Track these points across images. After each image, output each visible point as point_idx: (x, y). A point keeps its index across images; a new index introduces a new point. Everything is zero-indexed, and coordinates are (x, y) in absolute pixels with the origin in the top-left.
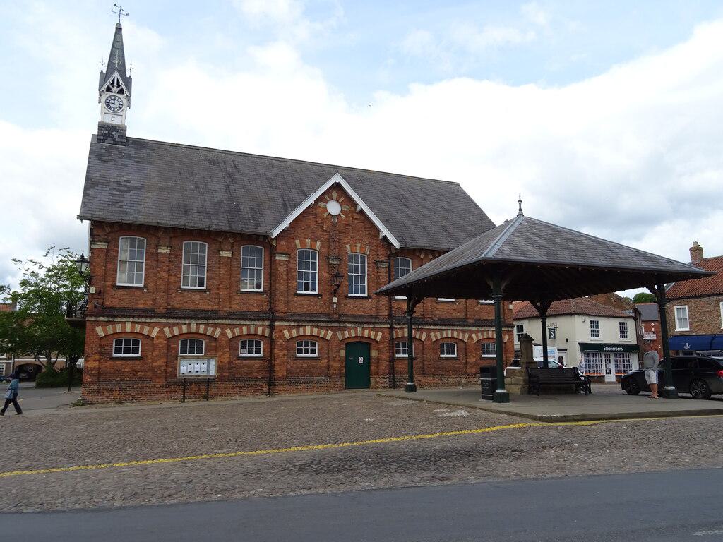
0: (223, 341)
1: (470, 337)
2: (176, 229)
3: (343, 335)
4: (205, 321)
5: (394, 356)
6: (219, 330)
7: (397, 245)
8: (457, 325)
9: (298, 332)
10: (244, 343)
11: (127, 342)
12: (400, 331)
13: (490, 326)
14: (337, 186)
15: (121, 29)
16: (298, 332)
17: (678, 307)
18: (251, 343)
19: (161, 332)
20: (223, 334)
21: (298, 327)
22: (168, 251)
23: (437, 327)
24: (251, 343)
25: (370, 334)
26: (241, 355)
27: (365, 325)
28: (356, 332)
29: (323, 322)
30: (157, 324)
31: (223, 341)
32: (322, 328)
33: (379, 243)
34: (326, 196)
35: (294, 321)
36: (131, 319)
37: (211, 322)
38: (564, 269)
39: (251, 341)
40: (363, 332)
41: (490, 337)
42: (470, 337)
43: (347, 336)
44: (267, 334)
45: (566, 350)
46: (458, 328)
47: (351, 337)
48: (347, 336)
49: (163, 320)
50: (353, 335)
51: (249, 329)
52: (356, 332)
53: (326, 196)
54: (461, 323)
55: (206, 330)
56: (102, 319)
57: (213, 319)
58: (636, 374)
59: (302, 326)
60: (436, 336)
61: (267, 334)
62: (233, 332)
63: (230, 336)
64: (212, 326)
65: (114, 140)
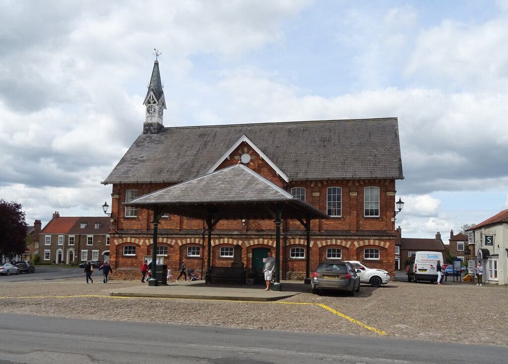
0: (176, 247)
1: (352, 244)
2: (142, 184)
3: (249, 243)
4: (166, 236)
5: (67, 265)
6: (174, 241)
7: (286, 179)
8: (340, 236)
9: (219, 241)
10: (190, 249)
11: (130, 247)
12: (292, 240)
13: (371, 236)
14: (244, 144)
15: (158, 64)
16: (219, 241)
17: (87, 243)
18: (194, 249)
19: (144, 242)
20: (176, 243)
21: (220, 238)
22: (118, 197)
23: (323, 237)
24: (194, 249)
25: (268, 242)
26: (188, 256)
27: (264, 237)
28: (258, 241)
29: (236, 235)
30: (142, 237)
31: (176, 247)
32: (235, 239)
33: (277, 179)
34: (251, 151)
35: (216, 234)
36: (130, 235)
37: (169, 236)
38: (194, 205)
39: (194, 248)
40: (263, 241)
41: (372, 244)
42: (352, 244)
43: (252, 244)
44: (201, 243)
45: (498, 255)
46: (342, 237)
47: (254, 245)
48: (252, 244)
49: (145, 236)
50: (256, 243)
51: (191, 240)
52: (258, 241)
53: (251, 151)
54: (344, 234)
55: (167, 241)
56: (116, 236)
57: (171, 234)
58: (166, 283)
59: (222, 238)
60: (322, 244)
61: (201, 243)
62: (182, 242)
63: (180, 244)
64: (170, 239)
65: (151, 131)
